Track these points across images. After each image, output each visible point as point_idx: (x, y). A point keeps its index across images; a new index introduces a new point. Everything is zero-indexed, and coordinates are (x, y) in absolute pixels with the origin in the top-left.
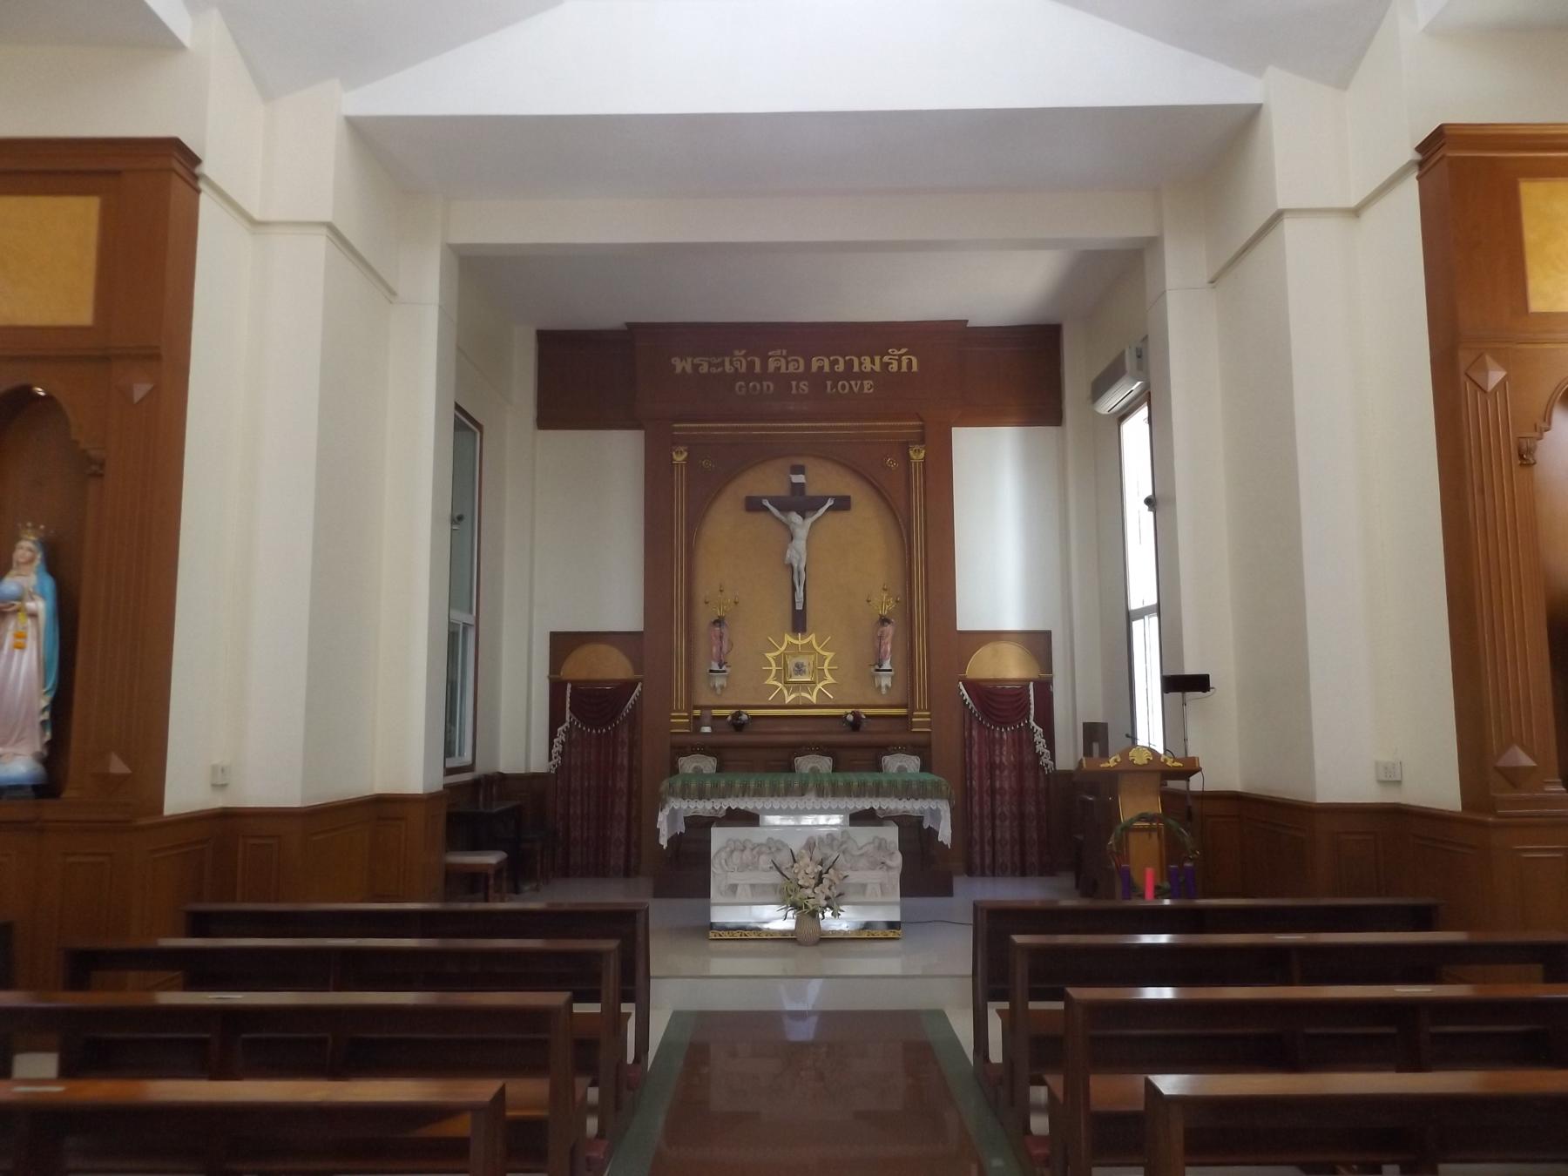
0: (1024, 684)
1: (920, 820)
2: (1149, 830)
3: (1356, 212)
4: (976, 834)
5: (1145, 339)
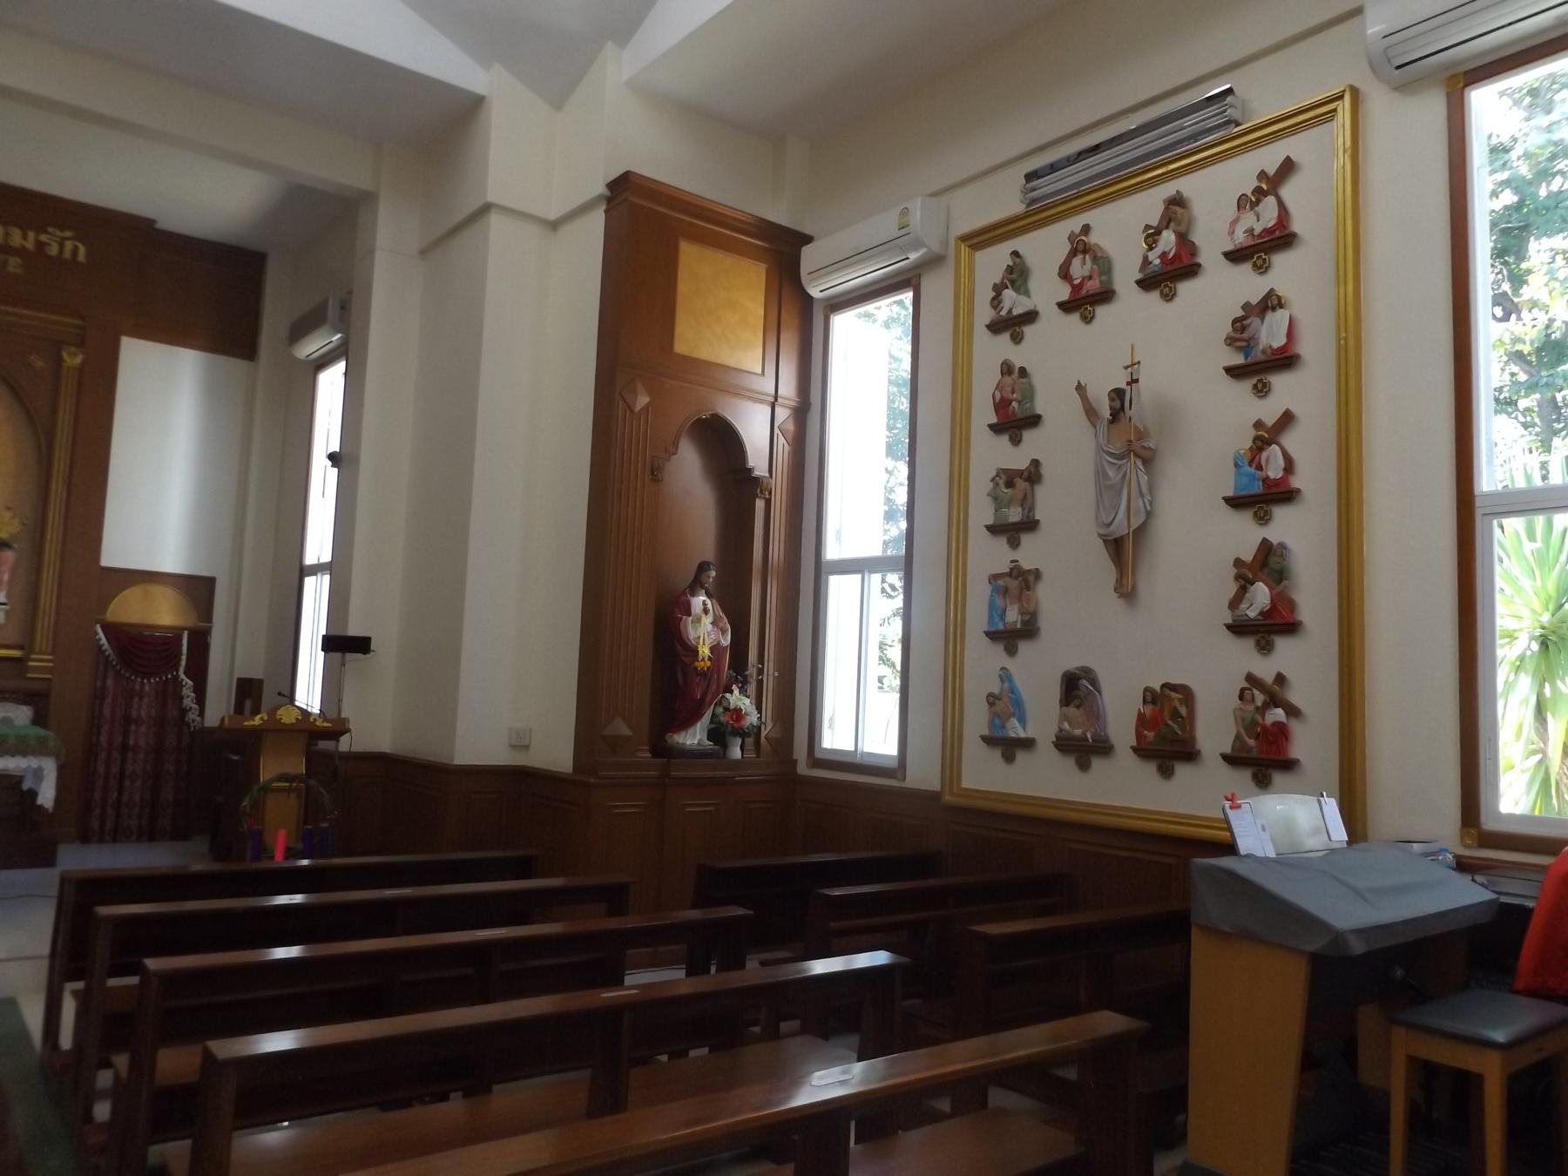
0: (177, 632)
1: (19, 780)
2: (288, 791)
3: (554, 225)
4: (97, 796)
5: (350, 293)
